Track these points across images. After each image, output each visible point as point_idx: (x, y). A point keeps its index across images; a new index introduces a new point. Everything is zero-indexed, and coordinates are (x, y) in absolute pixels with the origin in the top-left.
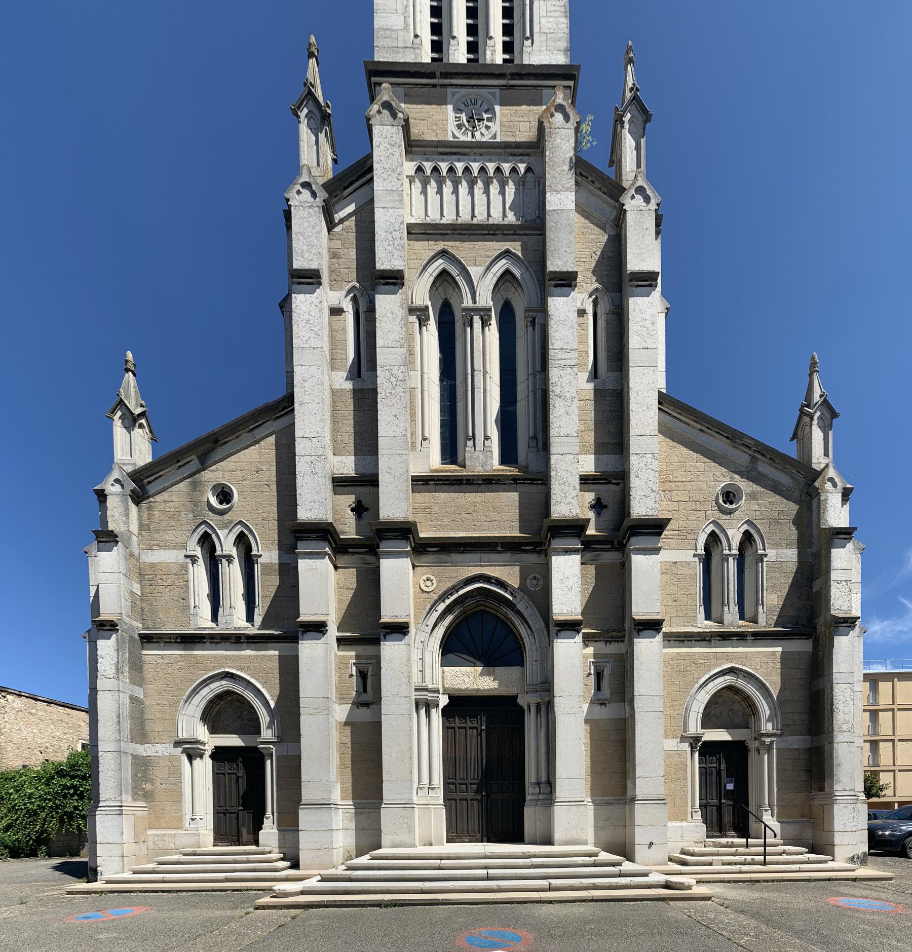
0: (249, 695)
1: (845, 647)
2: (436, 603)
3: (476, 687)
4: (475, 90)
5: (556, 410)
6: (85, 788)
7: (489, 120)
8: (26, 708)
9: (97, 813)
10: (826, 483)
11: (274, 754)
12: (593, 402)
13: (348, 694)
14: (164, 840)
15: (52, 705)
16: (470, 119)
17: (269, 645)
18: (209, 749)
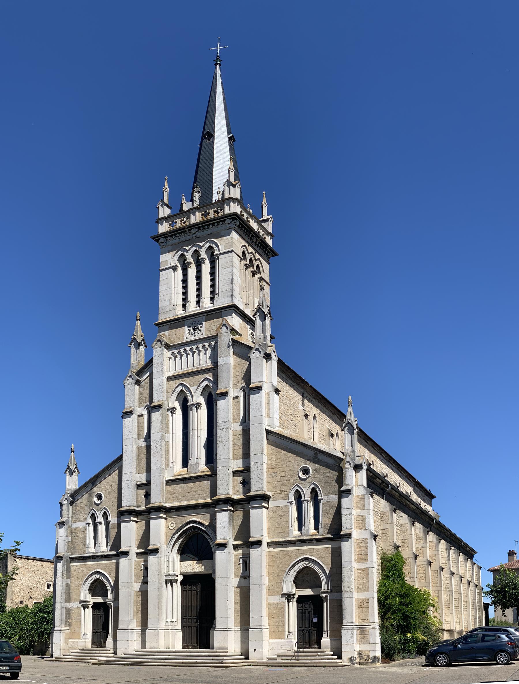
0: (104, 580)
1: (348, 548)
2: (174, 534)
3: (194, 571)
4: (195, 319)
5: (220, 448)
6: (49, 618)
7: (201, 327)
8: (24, 565)
9: (54, 631)
10: (346, 464)
11: (112, 606)
12: (242, 435)
13: (140, 578)
14: (74, 644)
15: (35, 561)
16: (194, 329)
17: (112, 558)
18: (91, 604)
